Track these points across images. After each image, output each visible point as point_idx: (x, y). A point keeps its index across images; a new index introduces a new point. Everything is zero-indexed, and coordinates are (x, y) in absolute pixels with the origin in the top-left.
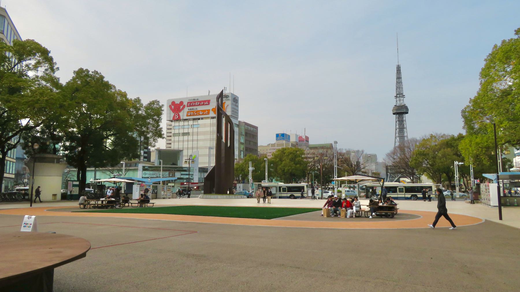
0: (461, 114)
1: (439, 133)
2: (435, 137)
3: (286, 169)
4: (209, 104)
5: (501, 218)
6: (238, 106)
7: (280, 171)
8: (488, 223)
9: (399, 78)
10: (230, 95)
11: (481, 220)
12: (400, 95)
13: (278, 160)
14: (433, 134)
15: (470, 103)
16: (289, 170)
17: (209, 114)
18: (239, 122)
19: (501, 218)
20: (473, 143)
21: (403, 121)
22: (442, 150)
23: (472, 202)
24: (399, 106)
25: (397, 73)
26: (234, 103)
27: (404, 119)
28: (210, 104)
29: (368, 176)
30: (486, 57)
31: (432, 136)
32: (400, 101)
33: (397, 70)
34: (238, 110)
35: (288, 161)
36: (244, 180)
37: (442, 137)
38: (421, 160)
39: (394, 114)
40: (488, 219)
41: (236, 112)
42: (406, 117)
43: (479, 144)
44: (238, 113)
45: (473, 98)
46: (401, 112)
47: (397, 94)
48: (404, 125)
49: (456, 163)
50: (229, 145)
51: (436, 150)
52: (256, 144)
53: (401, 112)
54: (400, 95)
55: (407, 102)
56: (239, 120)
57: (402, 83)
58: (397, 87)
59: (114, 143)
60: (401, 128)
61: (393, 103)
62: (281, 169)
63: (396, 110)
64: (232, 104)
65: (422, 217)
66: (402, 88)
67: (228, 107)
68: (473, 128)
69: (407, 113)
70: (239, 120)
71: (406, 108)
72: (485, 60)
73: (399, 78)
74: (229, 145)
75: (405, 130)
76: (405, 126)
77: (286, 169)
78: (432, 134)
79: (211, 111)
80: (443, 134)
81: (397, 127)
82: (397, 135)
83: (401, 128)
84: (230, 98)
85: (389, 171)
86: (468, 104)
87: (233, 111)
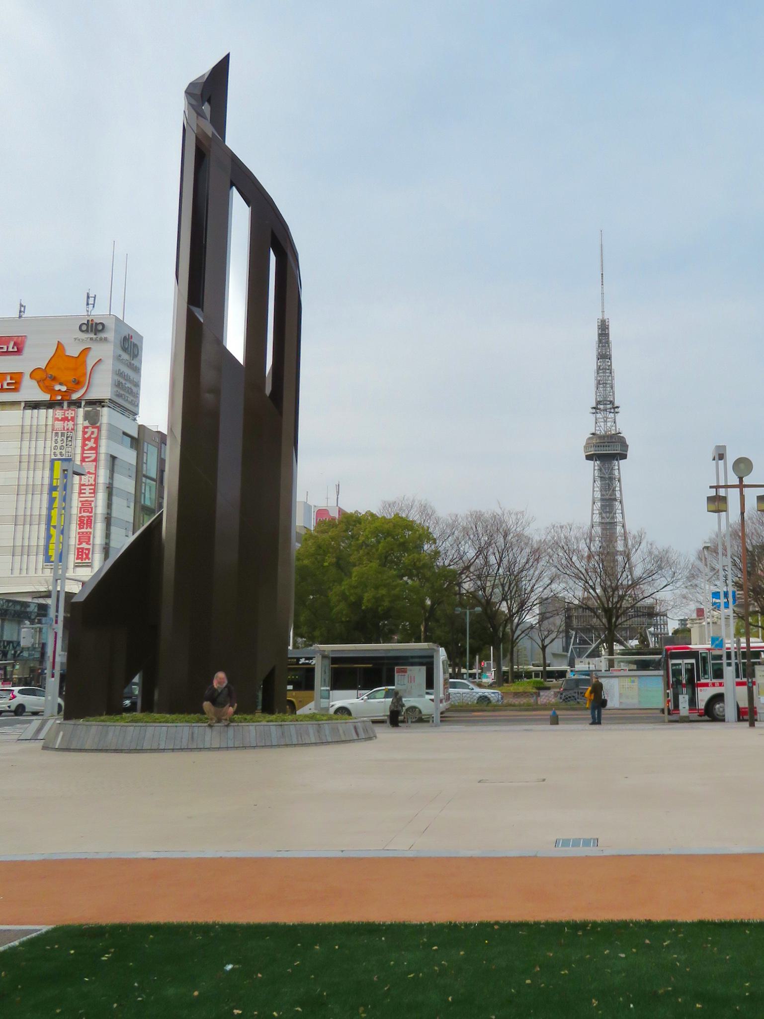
3: (367, 596)
4: (19, 351)
6: (137, 370)
7: (342, 605)
9: (604, 356)
10: (110, 324)
12: (605, 405)
13: (329, 560)
16: (378, 600)
17: (16, 390)
18: (142, 428)
21: (611, 479)
24: (601, 437)
25: (600, 341)
26: (125, 356)
28: (26, 351)
33: (600, 335)
34: (137, 385)
35: (375, 564)
39: (589, 457)
41: (130, 392)
44: (136, 396)
46: (607, 452)
47: (598, 403)
50: (235, 342)
53: (607, 452)
54: (605, 405)
56: (141, 420)
58: (599, 383)
59: (591, 1003)
61: (585, 426)
62: (344, 597)
63: (597, 446)
64: (118, 358)
67: (101, 367)
69: (624, 457)
70: (141, 420)
73: (604, 356)
74: (235, 342)
76: (618, 494)
77: (367, 596)
79: (27, 377)
81: (598, 495)
84: (110, 335)
85: (575, 622)
87: (118, 385)
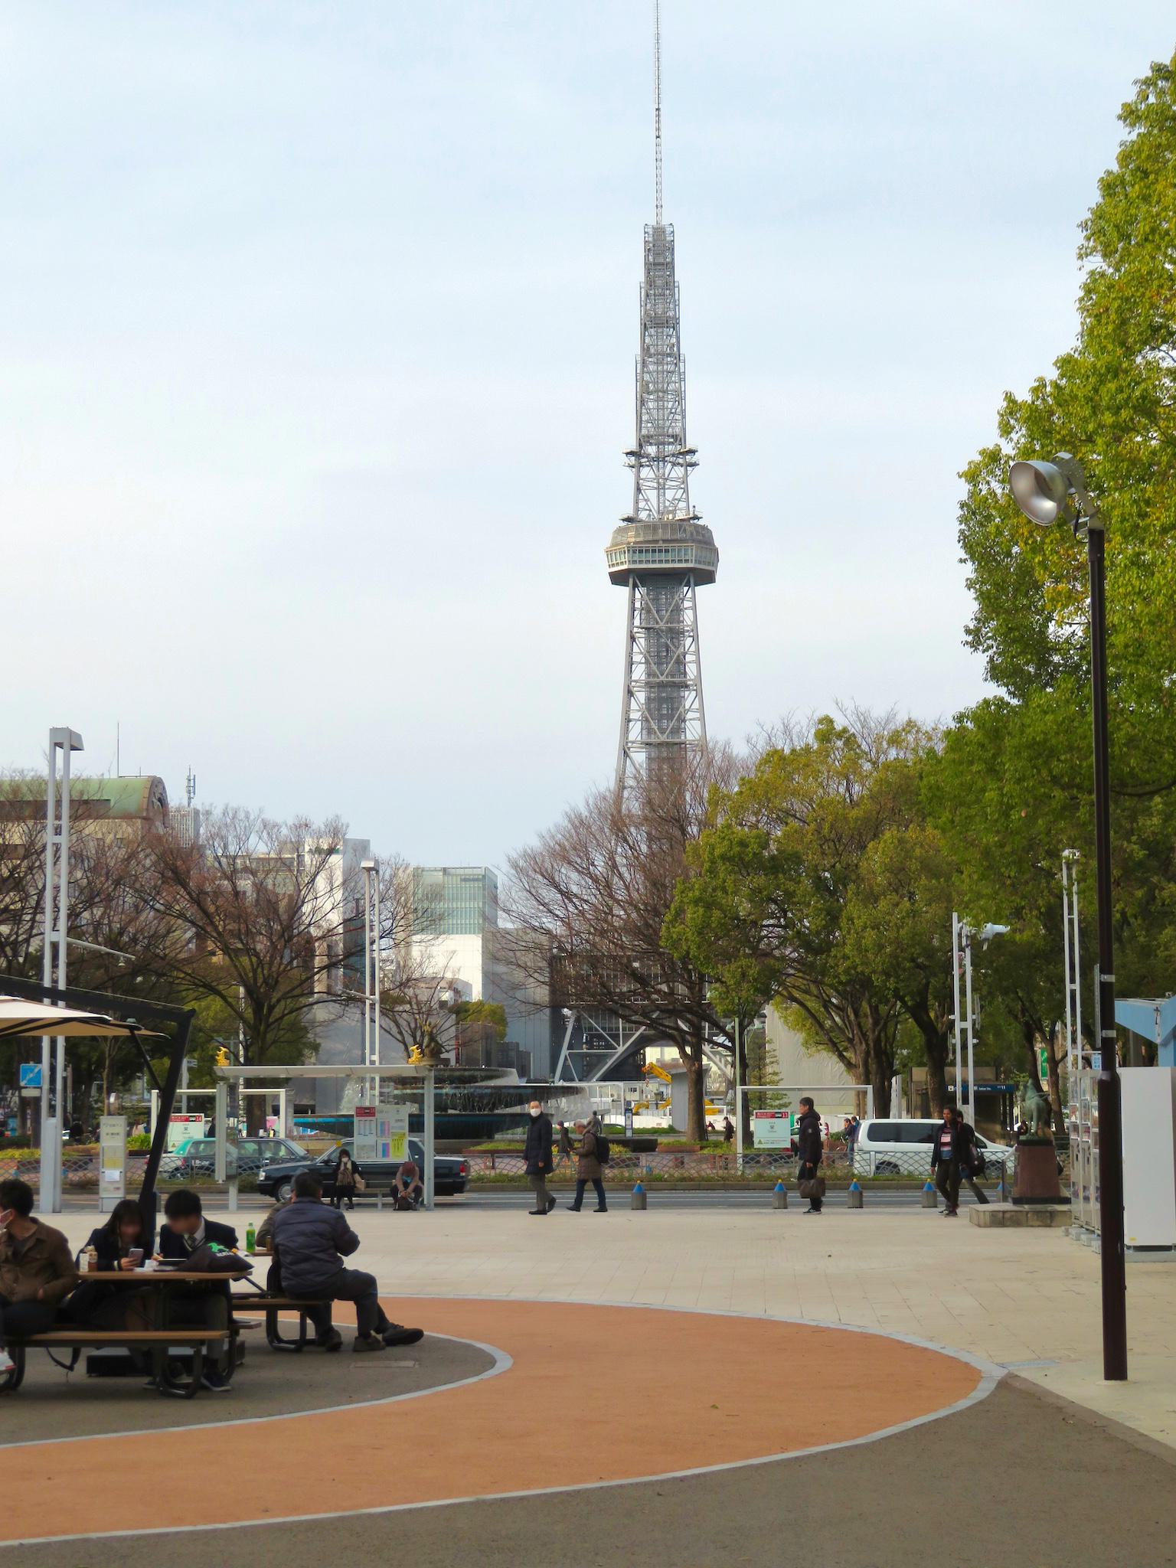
0: (954, 528)
1: (878, 711)
2: (850, 740)
5: (1116, 1366)
8: (1021, 1408)
9: (660, 319)
11: (970, 1375)
12: (661, 445)
14: (840, 723)
15: (1006, 430)
19: (1116, 1366)
20: (1008, 742)
22: (889, 835)
23: (542, 1212)
25: (650, 282)
27: (688, 616)
29: (35, 993)
30: (1130, 95)
31: (827, 732)
32: (661, 488)
36: (179, 1110)
37: (895, 740)
38: (744, 908)
39: (618, 578)
40: (1031, 1374)
42: (704, 603)
43: (1053, 753)
45: (1023, 396)
46: (666, 567)
48: (680, 662)
49: (960, 926)
51: (846, 836)
52: (485, 941)
53: (666, 567)
54: (661, 445)
55: (709, 496)
57: (678, 357)
60: (666, 684)
61: (609, 494)
63: (636, 550)
65: (504, 1363)
66: (680, 396)
68: (1040, 647)
69: (707, 577)
71: (704, 539)
72: (1130, 115)
73: (660, 319)
75: (689, 697)
76: (691, 670)
78: (828, 721)
80: (901, 719)
81: (639, 672)
82: (636, 731)
83: (666, 684)
86: (991, 438)
